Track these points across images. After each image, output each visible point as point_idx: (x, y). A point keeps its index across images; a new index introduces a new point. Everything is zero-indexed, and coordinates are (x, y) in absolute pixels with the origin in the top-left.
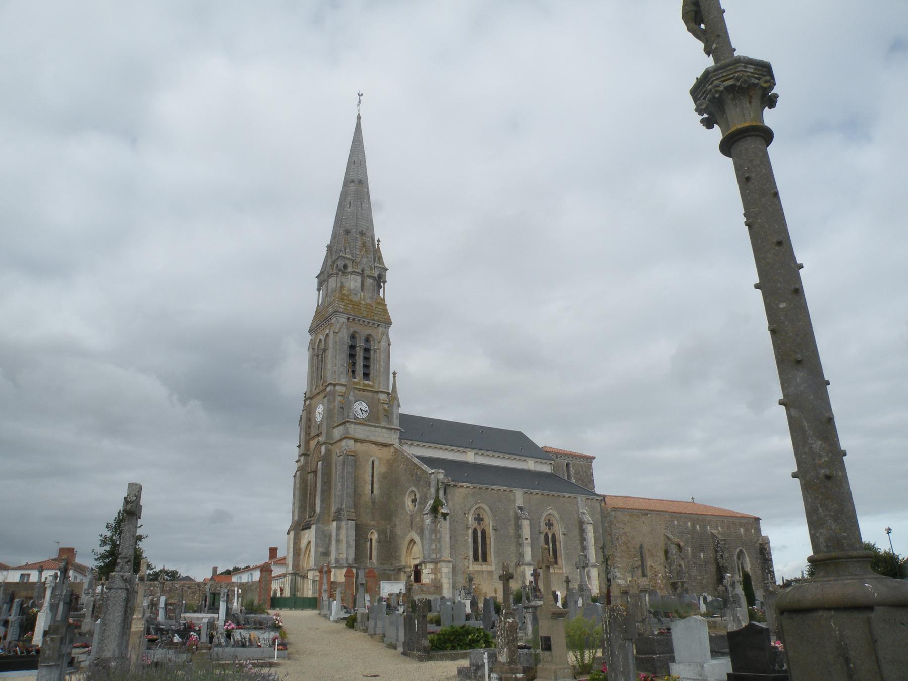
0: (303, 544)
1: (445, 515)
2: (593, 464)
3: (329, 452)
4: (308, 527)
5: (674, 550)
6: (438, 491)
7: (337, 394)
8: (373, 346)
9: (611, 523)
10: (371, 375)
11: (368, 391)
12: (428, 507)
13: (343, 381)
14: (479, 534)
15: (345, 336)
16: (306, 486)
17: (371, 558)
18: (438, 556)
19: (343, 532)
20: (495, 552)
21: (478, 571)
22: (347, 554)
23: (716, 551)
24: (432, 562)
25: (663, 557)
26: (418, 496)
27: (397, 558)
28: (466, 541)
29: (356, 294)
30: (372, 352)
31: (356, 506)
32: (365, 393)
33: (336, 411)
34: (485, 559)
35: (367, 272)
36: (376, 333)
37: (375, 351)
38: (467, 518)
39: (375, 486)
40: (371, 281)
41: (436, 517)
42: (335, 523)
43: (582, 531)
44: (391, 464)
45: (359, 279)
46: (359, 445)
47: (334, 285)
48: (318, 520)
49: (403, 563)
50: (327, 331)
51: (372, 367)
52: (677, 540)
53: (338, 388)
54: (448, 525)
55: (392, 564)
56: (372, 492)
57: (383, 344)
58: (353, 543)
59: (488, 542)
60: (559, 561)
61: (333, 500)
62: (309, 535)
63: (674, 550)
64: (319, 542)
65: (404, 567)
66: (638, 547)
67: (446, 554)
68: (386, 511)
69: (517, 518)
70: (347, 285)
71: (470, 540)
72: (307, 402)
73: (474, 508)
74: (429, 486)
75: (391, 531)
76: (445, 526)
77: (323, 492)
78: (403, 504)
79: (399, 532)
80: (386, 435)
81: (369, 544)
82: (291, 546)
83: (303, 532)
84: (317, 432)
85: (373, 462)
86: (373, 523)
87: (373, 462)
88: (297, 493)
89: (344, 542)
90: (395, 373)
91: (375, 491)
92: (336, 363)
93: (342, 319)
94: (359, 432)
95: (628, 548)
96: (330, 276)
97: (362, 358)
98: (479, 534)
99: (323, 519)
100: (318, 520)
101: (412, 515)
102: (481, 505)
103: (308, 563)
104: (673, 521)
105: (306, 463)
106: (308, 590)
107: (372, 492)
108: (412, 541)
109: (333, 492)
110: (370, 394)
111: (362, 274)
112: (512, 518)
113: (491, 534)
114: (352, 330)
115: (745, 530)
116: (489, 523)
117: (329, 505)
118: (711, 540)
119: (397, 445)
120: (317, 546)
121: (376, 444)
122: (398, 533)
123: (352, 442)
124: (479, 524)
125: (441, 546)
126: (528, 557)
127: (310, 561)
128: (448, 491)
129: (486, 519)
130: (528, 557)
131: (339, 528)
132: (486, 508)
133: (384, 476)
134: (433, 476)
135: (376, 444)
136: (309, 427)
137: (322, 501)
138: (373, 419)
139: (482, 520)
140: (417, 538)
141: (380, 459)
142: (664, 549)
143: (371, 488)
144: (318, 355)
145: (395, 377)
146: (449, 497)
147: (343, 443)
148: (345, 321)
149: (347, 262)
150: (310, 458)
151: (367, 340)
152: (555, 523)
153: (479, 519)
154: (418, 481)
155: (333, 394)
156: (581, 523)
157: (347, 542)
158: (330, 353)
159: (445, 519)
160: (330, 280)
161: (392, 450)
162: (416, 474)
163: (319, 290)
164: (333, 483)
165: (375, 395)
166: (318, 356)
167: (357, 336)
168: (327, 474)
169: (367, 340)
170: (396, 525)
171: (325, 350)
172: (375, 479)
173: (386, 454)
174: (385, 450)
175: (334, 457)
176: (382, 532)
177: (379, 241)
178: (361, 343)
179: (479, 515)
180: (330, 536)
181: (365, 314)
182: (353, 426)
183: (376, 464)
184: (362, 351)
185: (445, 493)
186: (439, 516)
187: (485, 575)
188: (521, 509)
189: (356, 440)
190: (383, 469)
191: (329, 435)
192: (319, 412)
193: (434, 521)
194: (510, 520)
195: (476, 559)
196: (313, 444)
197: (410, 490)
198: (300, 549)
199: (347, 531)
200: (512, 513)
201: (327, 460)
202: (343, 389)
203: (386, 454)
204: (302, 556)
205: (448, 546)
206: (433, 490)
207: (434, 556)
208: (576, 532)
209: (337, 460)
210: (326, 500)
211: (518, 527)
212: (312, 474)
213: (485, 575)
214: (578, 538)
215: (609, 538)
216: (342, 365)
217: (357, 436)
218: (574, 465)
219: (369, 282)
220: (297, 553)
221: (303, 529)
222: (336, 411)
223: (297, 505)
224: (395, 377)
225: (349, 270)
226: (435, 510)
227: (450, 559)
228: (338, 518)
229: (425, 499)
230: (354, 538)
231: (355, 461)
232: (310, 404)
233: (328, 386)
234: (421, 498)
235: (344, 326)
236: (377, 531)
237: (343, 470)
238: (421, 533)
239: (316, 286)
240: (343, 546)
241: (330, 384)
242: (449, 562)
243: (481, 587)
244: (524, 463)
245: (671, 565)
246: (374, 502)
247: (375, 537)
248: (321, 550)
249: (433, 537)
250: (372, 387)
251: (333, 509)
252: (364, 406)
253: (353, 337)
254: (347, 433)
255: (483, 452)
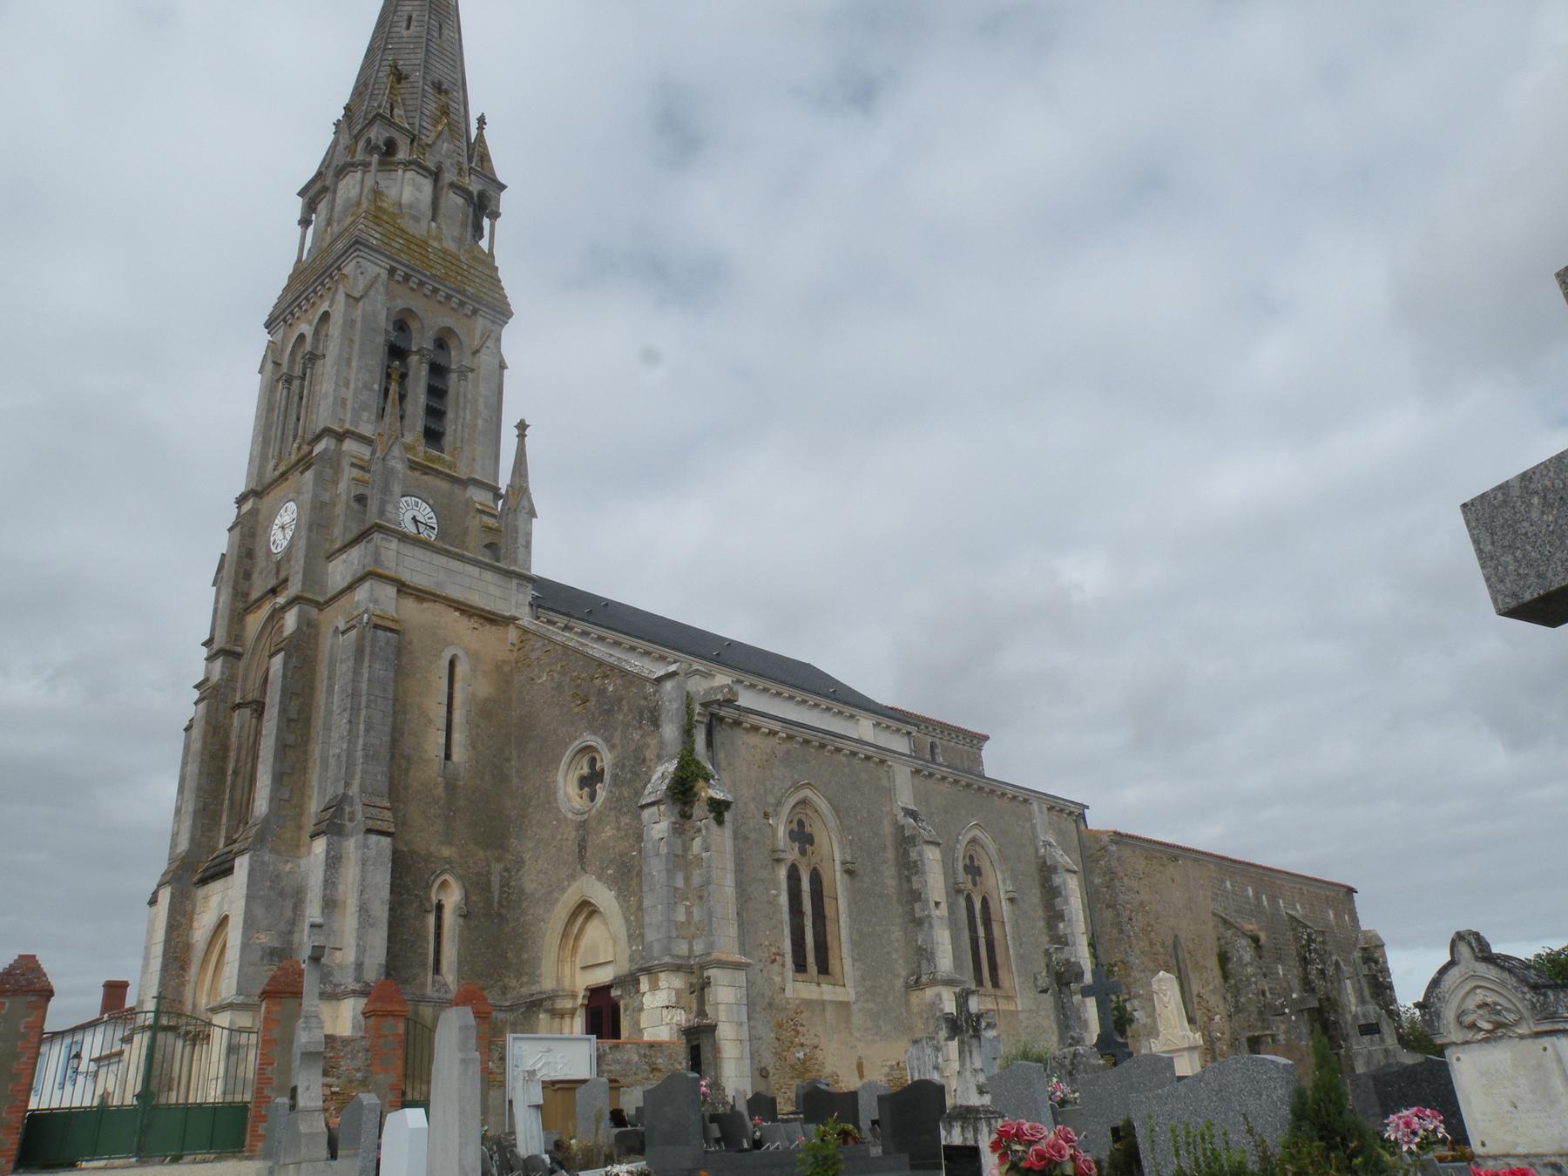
0: (204, 923)
1: (719, 809)
2: (983, 753)
3: (308, 629)
4: (223, 870)
5: (1244, 951)
6: (688, 732)
7: (345, 463)
8: (455, 359)
9: (1110, 872)
10: (448, 439)
11: (438, 473)
12: (663, 772)
13: (367, 429)
14: (806, 885)
15: (379, 309)
16: (225, 748)
17: (437, 969)
18: (699, 947)
19: (350, 874)
20: (855, 945)
21: (808, 1003)
22: (361, 949)
23: (1305, 962)
24: (677, 969)
25: (1217, 972)
26: (606, 760)
27: (527, 969)
28: (772, 902)
29: (417, 219)
30: (453, 377)
31: (396, 791)
32: (430, 480)
33: (340, 509)
34: (824, 968)
35: (449, 176)
36: (471, 330)
37: (463, 372)
38: (774, 829)
39: (457, 736)
40: (460, 201)
41: (685, 816)
42: (320, 846)
43: (1052, 895)
44: (505, 675)
45: (427, 185)
46: (410, 605)
47: (354, 193)
48: (261, 839)
49: (548, 984)
50: (325, 307)
51: (450, 415)
52: (1250, 927)
53: (349, 445)
54: (729, 844)
55: (504, 990)
56: (448, 757)
57: (485, 360)
58: (381, 912)
59: (829, 911)
60: (1003, 975)
61: (314, 777)
62: (227, 899)
63: (1244, 951)
64: (259, 911)
65: (553, 997)
66: (1170, 942)
67: (727, 943)
68: (490, 814)
69: (905, 841)
70: (392, 193)
71: (784, 899)
72: (247, 507)
73: (793, 801)
74: (656, 723)
75: (505, 884)
76: (716, 845)
77: (282, 748)
78: (551, 792)
79: (530, 880)
80: (493, 589)
81: (432, 919)
82: (160, 935)
83: (201, 892)
84: (272, 583)
85: (452, 664)
86: (446, 852)
87: (452, 664)
88: (193, 768)
89: (352, 904)
90: (522, 427)
91: (458, 754)
92: (343, 388)
93: (374, 268)
94: (420, 568)
95: (1152, 944)
96: (341, 172)
97: (421, 411)
98: (806, 885)
99: (277, 836)
100: (261, 839)
101: (582, 825)
102: (806, 793)
103: (213, 989)
104: (1223, 882)
105: (229, 680)
106: (208, 1078)
107: (448, 757)
108: (586, 909)
109: (316, 751)
110: (444, 485)
111: (436, 176)
112: (889, 841)
113: (837, 882)
114: (400, 304)
115: (1336, 915)
116: (832, 850)
117: (301, 790)
118: (1290, 933)
119: (526, 620)
120: (249, 924)
121: (465, 610)
122: (529, 887)
123: (391, 591)
124: (803, 852)
125: (710, 914)
126: (945, 962)
127: (224, 979)
128: (718, 737)
129: (821, 838)
130: (945, 962)
131: (333, 861)
132: (823, 805)
133: (486, 711)
134: (669, 685)
135: (465, 610)
136: (248, 575)
137: (278, 779)
138: (448, 543)
139: (810, 839)
140: (604, 896)
141: (475, 657)
142: (1216, 950)
143: (445, 744)
144: (289, 375)
145: (522, 436)
146: (721, 755)
147: (362, 593)
148: (384, 274)
149: (396, 135)
150: (242, 664)
151: (441, 344)
152: (986, 868)
153: (802, 837)
154: (609, 712)
155: (332, 461)
156: (1046, 871)
157: (363, 909)
158: (327, 369)
159: (720, 821)
160: (342, 185)
161: (512, 634)
162: (602, 692)
163: (305, 222)
164: (318, 723)
165: (457, 489)
166: (289, 381)
167: (414, 325)
168: (300, 692)
169: (441, 344)
170: (520, 863)
171: (313, 358)
172: (458, 716)
173: (495, 644)
174: (490, 631)
175: (326, 643)
176: (476, 886)
177: (482, 121)
178: (421, 341)
179: (801, 823)
180: (298, 897)
181: (439, 271)
182: (394, 544)
183: (461, 669)
184: (424, 371)
185: (710, 744)
186: (700, 810)
187: (830, 1012)
188: (909, 813)
189: (403, 588)
190: (484, 689)
191: (312, 574)
192: (284, 525)
193: (678, 830)
194: (884, 848)
195: (800, 966)
196: (255, 621)
197: (577, 745)
198: (188, 947)
199: (363, 870)
200: (887, 829)
201: (301, 650)
202: (364, 451)
203: (495, 644)
204: (194, 969)
205: (732, 910)
206: (670, 731)
207: (682, 948)
208: (1034, 897)
209: (335, 646)
210: (291, 772)
211: (909, 868)
212: (247, 712)
213: (830, 1012)
214: (1040, 913)
215: (1109, 915)
216: (367, 386)
217: (407, 577)
218: (945, 750)
219: (453, 201)
220: (177, 957)
221: (204, 881)
222: (340, 509)
223: (189, 807)
224: (522, 436)
225: (402, 155)
226: (682, 791)
227: (737, 958)
228: (332, 825)
229: (634, 768)
230: (385, 893)
231: (400, 651)
232: (254, 512)
233: (318, 438)
234: (619, 765)
235: (380, 286)
236: (460, 878)
237: (356, 672)
238: (626, 876)
239: (297, 214)
240: (349, 922)
241: (327, 431)
242: (738, 966)
243: (820, 1055)
244: (850, 724)
245: (1236, 992)
246: (451, 786)
247: (452, 898)
248: (264, 939)
249: (680, 883)
250: (451, 466)
251: (314, 806)
252: (425, 512)
253: (401, 325)
254: (377, 561)
255: (755, 680)
